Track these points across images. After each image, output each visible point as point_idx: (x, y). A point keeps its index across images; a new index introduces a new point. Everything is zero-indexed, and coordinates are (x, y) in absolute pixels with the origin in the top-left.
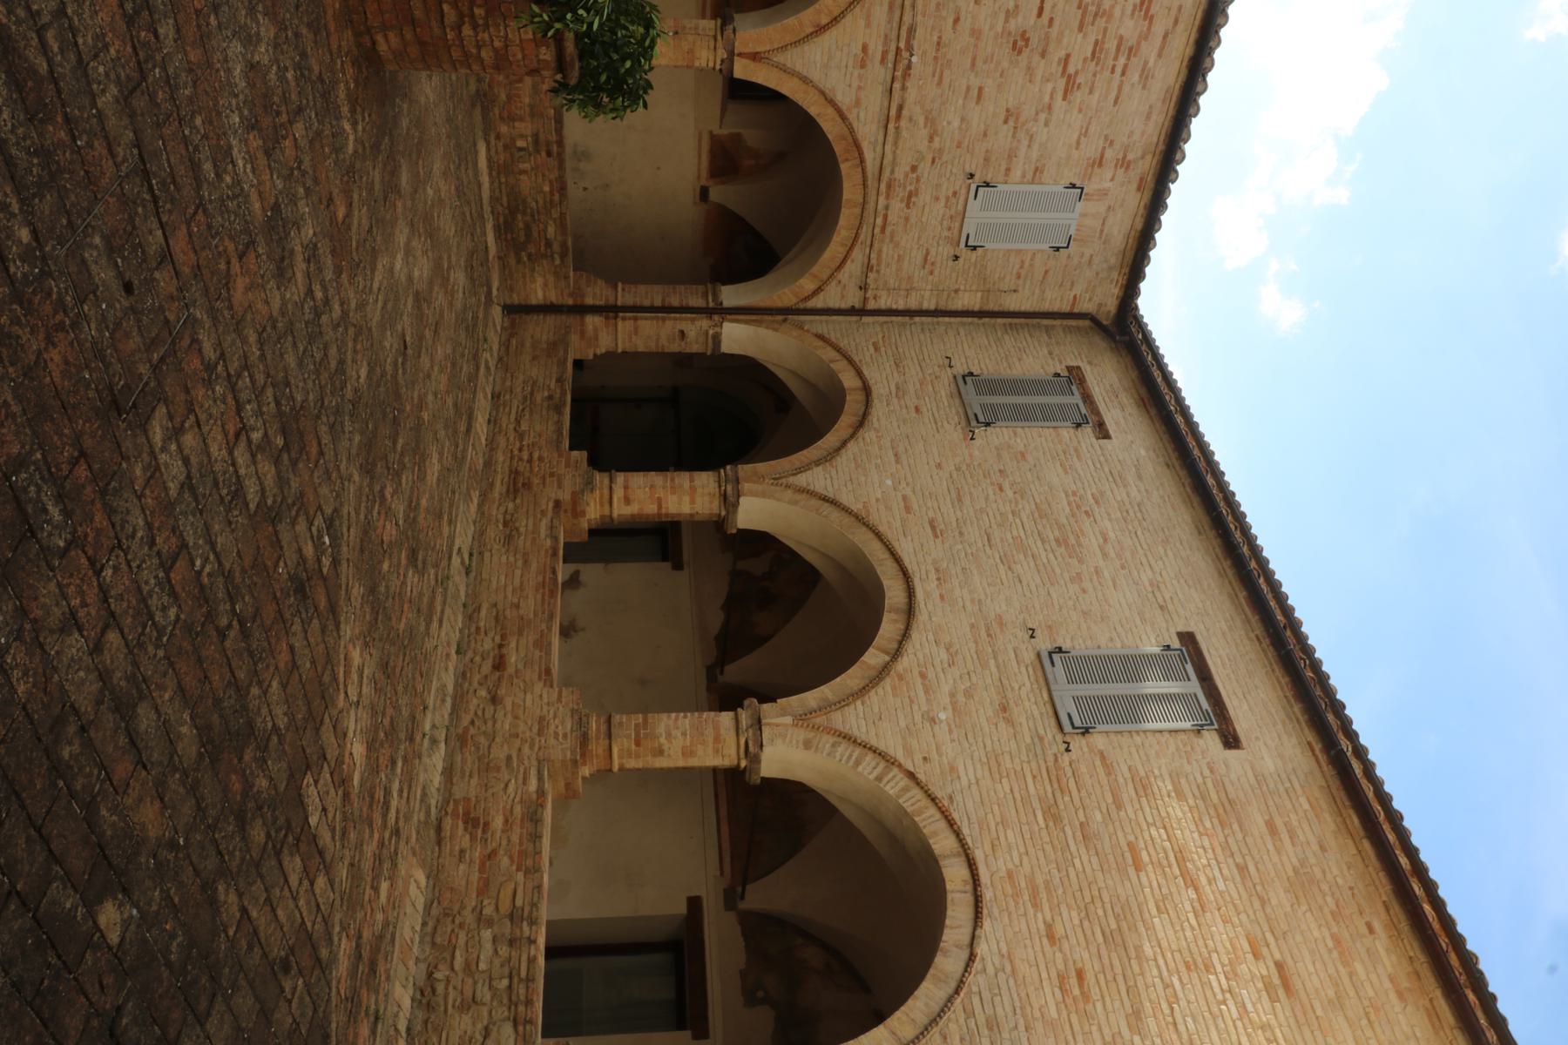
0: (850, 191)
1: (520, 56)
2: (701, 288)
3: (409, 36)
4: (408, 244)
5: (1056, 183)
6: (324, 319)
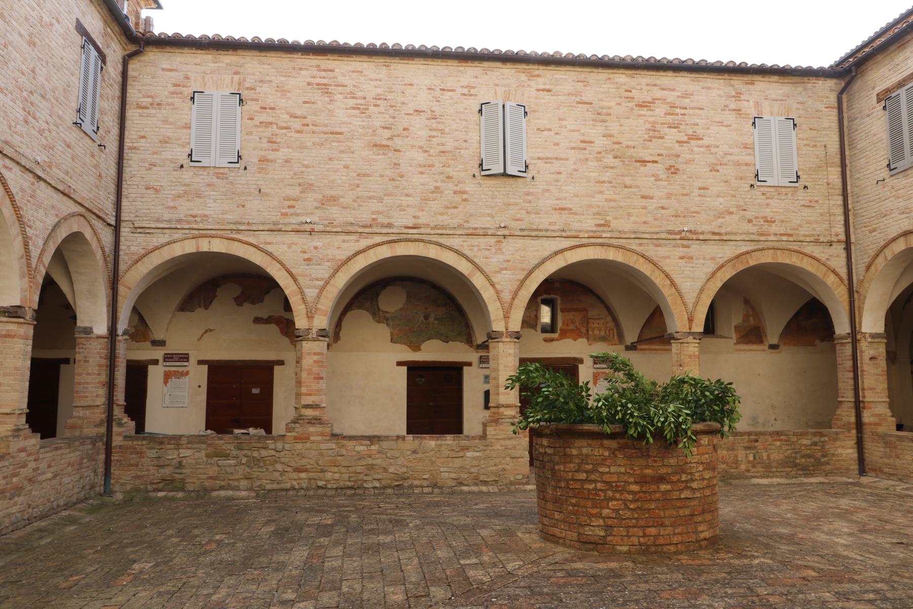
0: (766, 258)
1: (707, 456)
2: (838, 347)
3: (699, 519)
4: (827, 534)
5: (753, 134)
6: (889, 595)
